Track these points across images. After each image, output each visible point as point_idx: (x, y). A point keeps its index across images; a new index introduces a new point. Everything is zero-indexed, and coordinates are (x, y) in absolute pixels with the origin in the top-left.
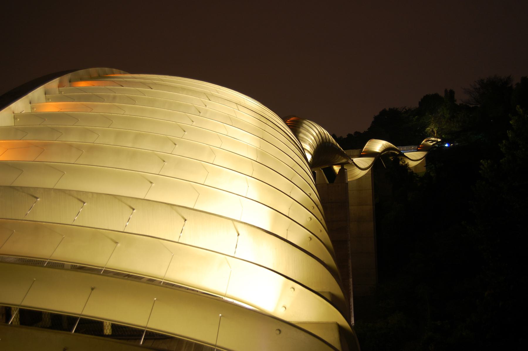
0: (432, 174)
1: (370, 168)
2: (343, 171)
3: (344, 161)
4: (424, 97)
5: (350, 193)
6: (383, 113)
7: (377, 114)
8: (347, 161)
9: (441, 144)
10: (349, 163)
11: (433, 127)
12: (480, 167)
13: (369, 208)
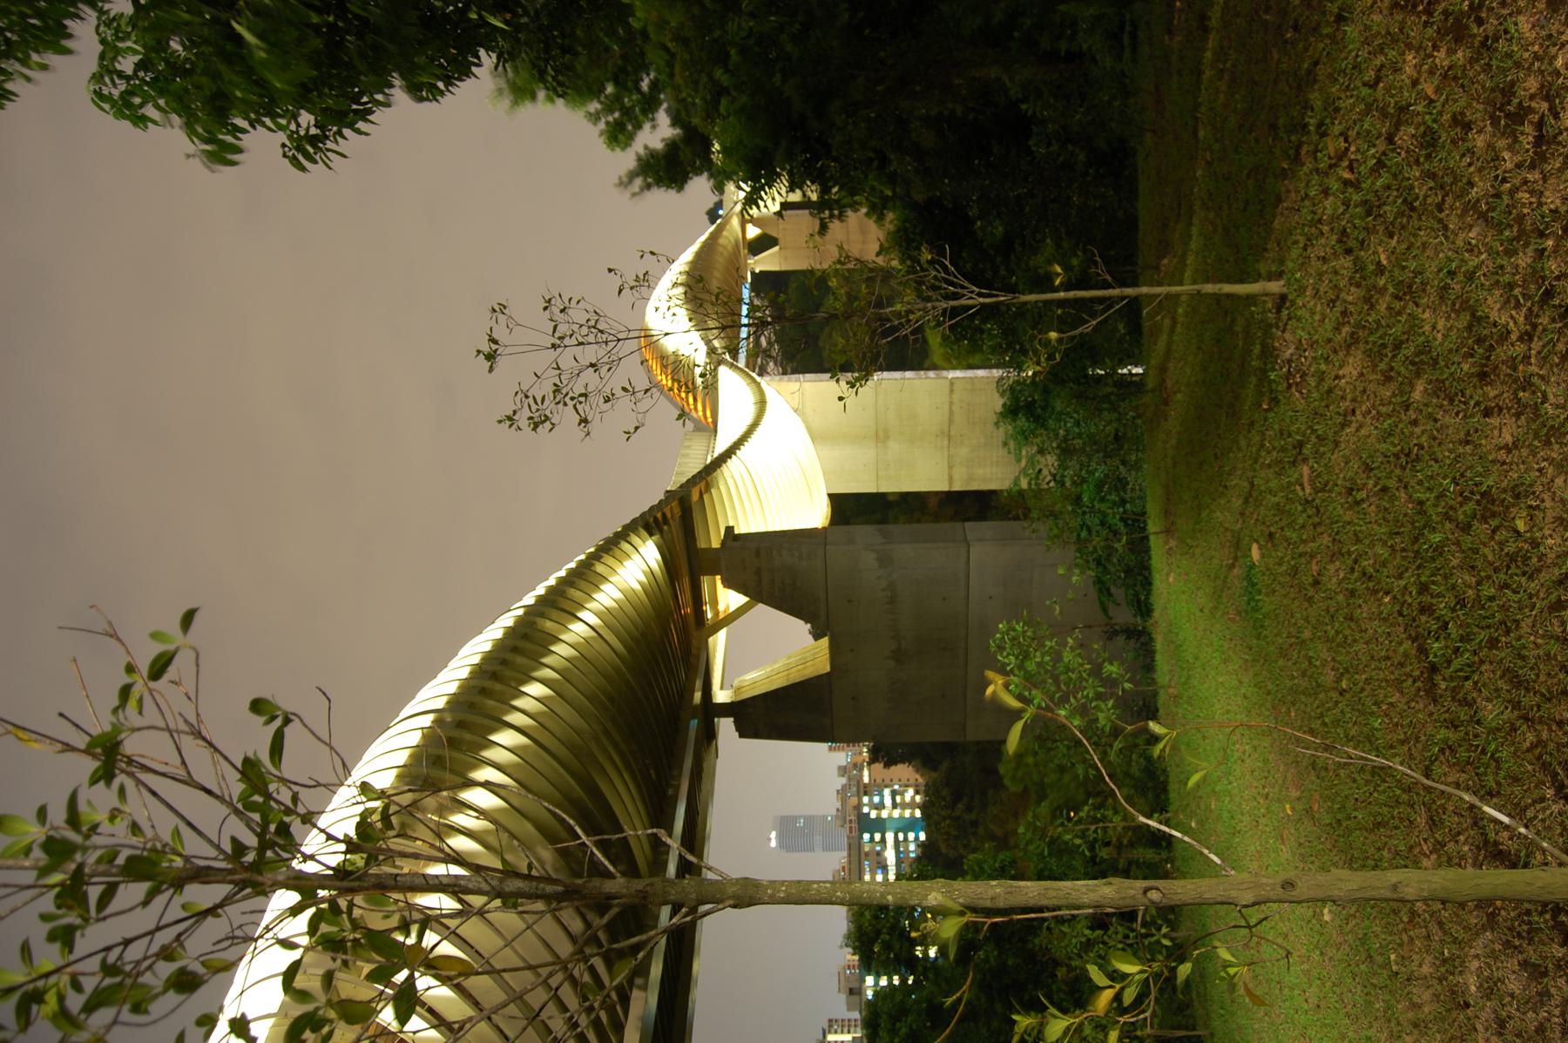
1: (758, 379)
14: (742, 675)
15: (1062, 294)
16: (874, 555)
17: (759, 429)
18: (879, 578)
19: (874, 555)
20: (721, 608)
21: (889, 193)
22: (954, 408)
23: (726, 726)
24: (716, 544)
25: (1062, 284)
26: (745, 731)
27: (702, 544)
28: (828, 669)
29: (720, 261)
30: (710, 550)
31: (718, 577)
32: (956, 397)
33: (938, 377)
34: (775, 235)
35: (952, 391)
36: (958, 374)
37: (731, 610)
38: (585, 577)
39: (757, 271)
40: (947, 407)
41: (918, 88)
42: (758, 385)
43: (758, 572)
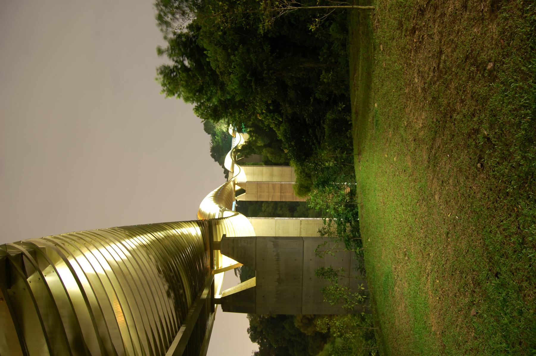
0: (248, 130)
2: (238, 184)
3: (232, 183)
4: (205, 131)
5: (252, 180)
6: (213, 156)
7: (213, 160)
8: (232, 181)
9: (258, 113)
10: (234, 180)
11: (223, 127)
12: (50, 279)
13: (265, 169)
14: (225, 290)
15: (319, 7)
16: (272, 243)
17: (234, 273)
18: (274, 251)
19: (272, 243)
20: (220, 266)
21: (281, 120)
22: (301, 230)
23: (219, 308)
24: (219, 240)
25: (318, 4)
26: (225, 309)
27: (215, 240)
28: (255, 285)
29: (226, 193)
30: (217, 242)
31: (219, 251)
32: (302, 226)
33: (296, 219)
34: (245, 189)
35: (301, 224)
36: (303, 218)
37: (223, 268)
38: (178, 224)
39: (238, 200)
40: (299, 229)
41: (289, 68)
43: (233, 248)
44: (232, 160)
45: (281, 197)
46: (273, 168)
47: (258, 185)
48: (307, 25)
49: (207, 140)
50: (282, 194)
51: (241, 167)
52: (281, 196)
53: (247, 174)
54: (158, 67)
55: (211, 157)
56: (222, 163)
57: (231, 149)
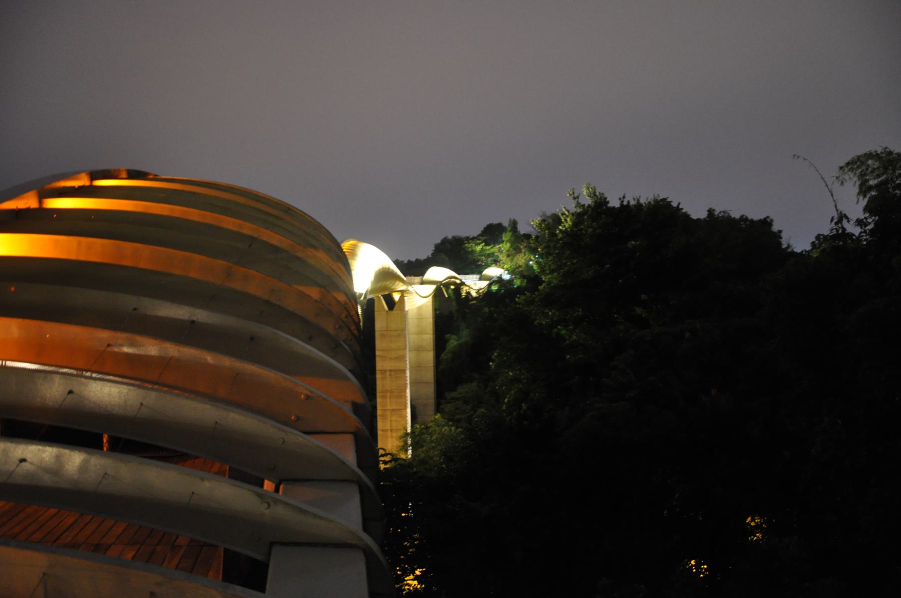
1: (431, 296)
2: (402, 298)
6: (445, 241)
7: (439, 241)
34: (395, 309)
42: (430, 295)
44: (441, 280)
45: (384, 372)
46: (430, 351)
47: (401, 333)
48: (538, 272)
49: (842, 164)
50: (388, 373)
51: (430, 299)
52: (385, 371)
53: (420, 308)
54: (435, 243)
55: (442, 237)
56: (434, 260)
57: (459, 274)
